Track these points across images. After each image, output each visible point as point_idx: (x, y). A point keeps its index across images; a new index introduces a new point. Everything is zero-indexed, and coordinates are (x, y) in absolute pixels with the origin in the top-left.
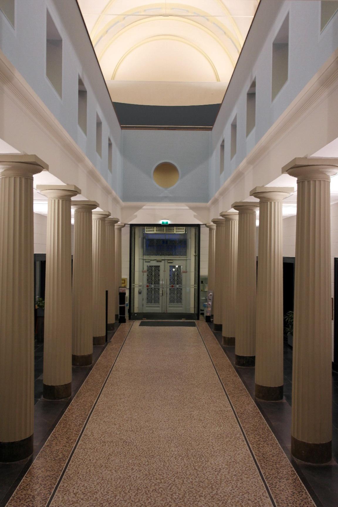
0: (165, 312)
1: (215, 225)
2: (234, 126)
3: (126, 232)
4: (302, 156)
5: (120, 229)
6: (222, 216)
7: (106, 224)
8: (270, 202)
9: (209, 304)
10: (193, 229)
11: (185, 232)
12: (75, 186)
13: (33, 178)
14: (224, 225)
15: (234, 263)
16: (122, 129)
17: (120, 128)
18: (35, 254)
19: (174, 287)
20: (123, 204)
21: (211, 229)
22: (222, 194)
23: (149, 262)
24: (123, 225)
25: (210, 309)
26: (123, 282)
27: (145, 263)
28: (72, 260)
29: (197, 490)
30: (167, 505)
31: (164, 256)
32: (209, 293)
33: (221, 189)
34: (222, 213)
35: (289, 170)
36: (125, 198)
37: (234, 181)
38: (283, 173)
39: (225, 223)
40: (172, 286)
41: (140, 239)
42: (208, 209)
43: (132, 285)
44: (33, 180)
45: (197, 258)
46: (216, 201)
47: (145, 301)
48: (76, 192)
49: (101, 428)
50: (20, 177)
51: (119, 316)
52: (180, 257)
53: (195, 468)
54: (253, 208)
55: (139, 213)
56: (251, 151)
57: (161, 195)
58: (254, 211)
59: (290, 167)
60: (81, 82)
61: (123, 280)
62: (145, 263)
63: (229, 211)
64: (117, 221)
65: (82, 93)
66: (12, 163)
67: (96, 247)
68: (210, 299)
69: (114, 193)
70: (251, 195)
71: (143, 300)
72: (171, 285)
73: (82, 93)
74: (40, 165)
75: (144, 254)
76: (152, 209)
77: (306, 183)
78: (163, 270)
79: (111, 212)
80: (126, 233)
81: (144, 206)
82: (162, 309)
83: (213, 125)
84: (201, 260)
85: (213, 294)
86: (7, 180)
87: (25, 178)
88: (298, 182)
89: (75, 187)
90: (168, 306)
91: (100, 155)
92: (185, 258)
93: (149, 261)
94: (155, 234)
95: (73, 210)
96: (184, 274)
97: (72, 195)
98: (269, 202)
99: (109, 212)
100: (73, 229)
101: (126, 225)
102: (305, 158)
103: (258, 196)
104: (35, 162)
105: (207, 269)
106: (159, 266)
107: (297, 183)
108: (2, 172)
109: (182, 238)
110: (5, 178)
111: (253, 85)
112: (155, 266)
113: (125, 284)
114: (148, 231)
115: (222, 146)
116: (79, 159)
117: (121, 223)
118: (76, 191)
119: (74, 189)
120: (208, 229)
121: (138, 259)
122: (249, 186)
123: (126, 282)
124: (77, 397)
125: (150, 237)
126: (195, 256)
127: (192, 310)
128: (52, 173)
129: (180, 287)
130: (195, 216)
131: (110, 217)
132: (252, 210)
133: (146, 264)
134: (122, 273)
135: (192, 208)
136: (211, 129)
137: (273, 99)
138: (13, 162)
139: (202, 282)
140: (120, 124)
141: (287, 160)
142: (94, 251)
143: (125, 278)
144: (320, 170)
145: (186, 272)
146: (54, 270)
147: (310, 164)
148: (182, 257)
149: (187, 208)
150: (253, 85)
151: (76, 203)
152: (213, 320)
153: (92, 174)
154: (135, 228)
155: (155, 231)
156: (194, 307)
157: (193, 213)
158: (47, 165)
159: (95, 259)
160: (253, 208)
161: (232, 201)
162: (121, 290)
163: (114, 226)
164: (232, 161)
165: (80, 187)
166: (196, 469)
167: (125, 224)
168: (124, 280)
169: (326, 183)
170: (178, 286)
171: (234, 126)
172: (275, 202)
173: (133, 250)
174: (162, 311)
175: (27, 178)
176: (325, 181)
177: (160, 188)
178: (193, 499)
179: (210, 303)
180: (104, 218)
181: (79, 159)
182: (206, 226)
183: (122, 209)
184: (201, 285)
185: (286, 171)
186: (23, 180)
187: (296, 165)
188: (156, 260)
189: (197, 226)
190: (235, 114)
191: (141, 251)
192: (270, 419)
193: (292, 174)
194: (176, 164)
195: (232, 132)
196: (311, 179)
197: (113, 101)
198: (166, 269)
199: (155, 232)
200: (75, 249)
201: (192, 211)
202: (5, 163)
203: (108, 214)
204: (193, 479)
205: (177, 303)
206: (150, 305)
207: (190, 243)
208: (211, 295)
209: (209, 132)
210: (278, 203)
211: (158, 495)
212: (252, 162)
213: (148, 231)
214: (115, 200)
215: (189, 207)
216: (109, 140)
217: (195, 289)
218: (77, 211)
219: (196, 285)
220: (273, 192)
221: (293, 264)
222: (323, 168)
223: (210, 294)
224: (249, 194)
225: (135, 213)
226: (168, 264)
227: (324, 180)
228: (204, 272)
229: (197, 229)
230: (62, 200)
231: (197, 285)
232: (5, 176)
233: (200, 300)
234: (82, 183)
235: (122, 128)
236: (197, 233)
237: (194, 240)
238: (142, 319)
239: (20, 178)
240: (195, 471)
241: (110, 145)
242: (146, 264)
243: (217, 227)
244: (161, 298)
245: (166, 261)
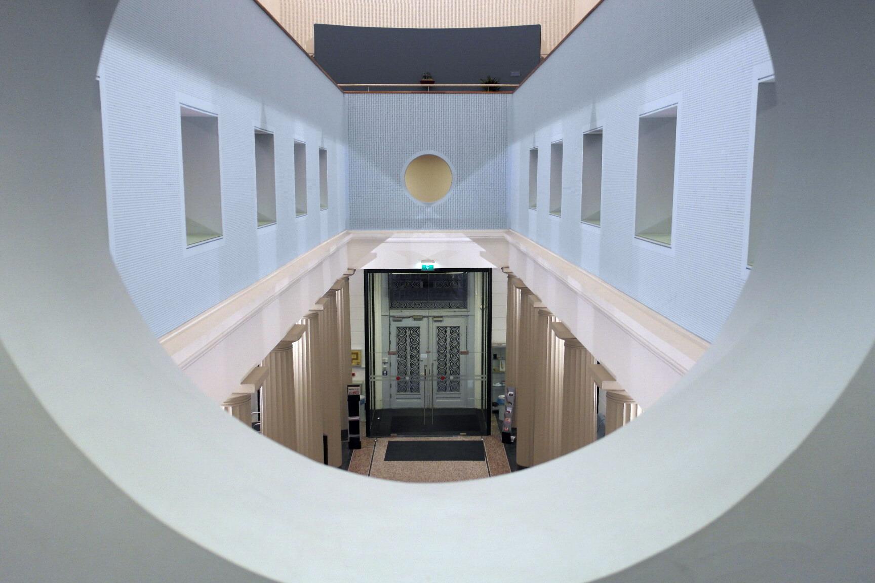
0: (431, 407)
8: (627, 404)
9: (509, 412)
15: (554, 383)
19: (445, 380)
23: (401, 321)
25: (510, 420)
26: (355, 356)
27: (392, 323)
32: (508, 392)
40: (443, 378)
43: (370, 376)
45: (486, 312)
47: (394, 389)
52: (455, 312)
55: (379, 250)
57: (420, 217)
61: (353, 353)
62: (392, 323)
68: (510, 403)
71: (391, 387)
72: (440, 376)
75: (391, 307)
76: (405, 242)
78: (426, 350)
81: (389, 237)
82: (425, 402)
84: (493, 328)
85: (515, 392)
90: (435, 396)
92: (465, 314)
93: (400, 319)
105: (505, 332)
106: (419, 328)
112: (410, 328)
113: (359, 361)
121: (381, 317)
123: (359, 358)
126: (483, 310)
127: (477, 402)
129: (455, 380)
130: (482, 254)
133: (395, 325)
135: (477, 240)
139: (495, 356)
142: (299, 420)
143: (357, 350)
145: (466, 353)
149: (468, 239)
152: (515, 440)
156: (481, 398)
162: (353, 390)
168: (357, 354)
170: (452, 378)
173: (371, 298)
174: (425, 406)
177: (419, 203)
179: (510, 409)
184: (494, 363)
188: (412, 317)
198: (430, 346)
201: (476, 244)
205: (451, 391)
206: (403, 395)
208: (512, 395)
217: (482, 382)
219: (485, 376)
223: (510, 393)
225: (374, 248)
228: (499, 336)
231: (486, 376)
233: (492, 387)
237: (481, 280)
238: (390, 435)
242: (395, 325)
244: (422, 383)
245: (431, 319)
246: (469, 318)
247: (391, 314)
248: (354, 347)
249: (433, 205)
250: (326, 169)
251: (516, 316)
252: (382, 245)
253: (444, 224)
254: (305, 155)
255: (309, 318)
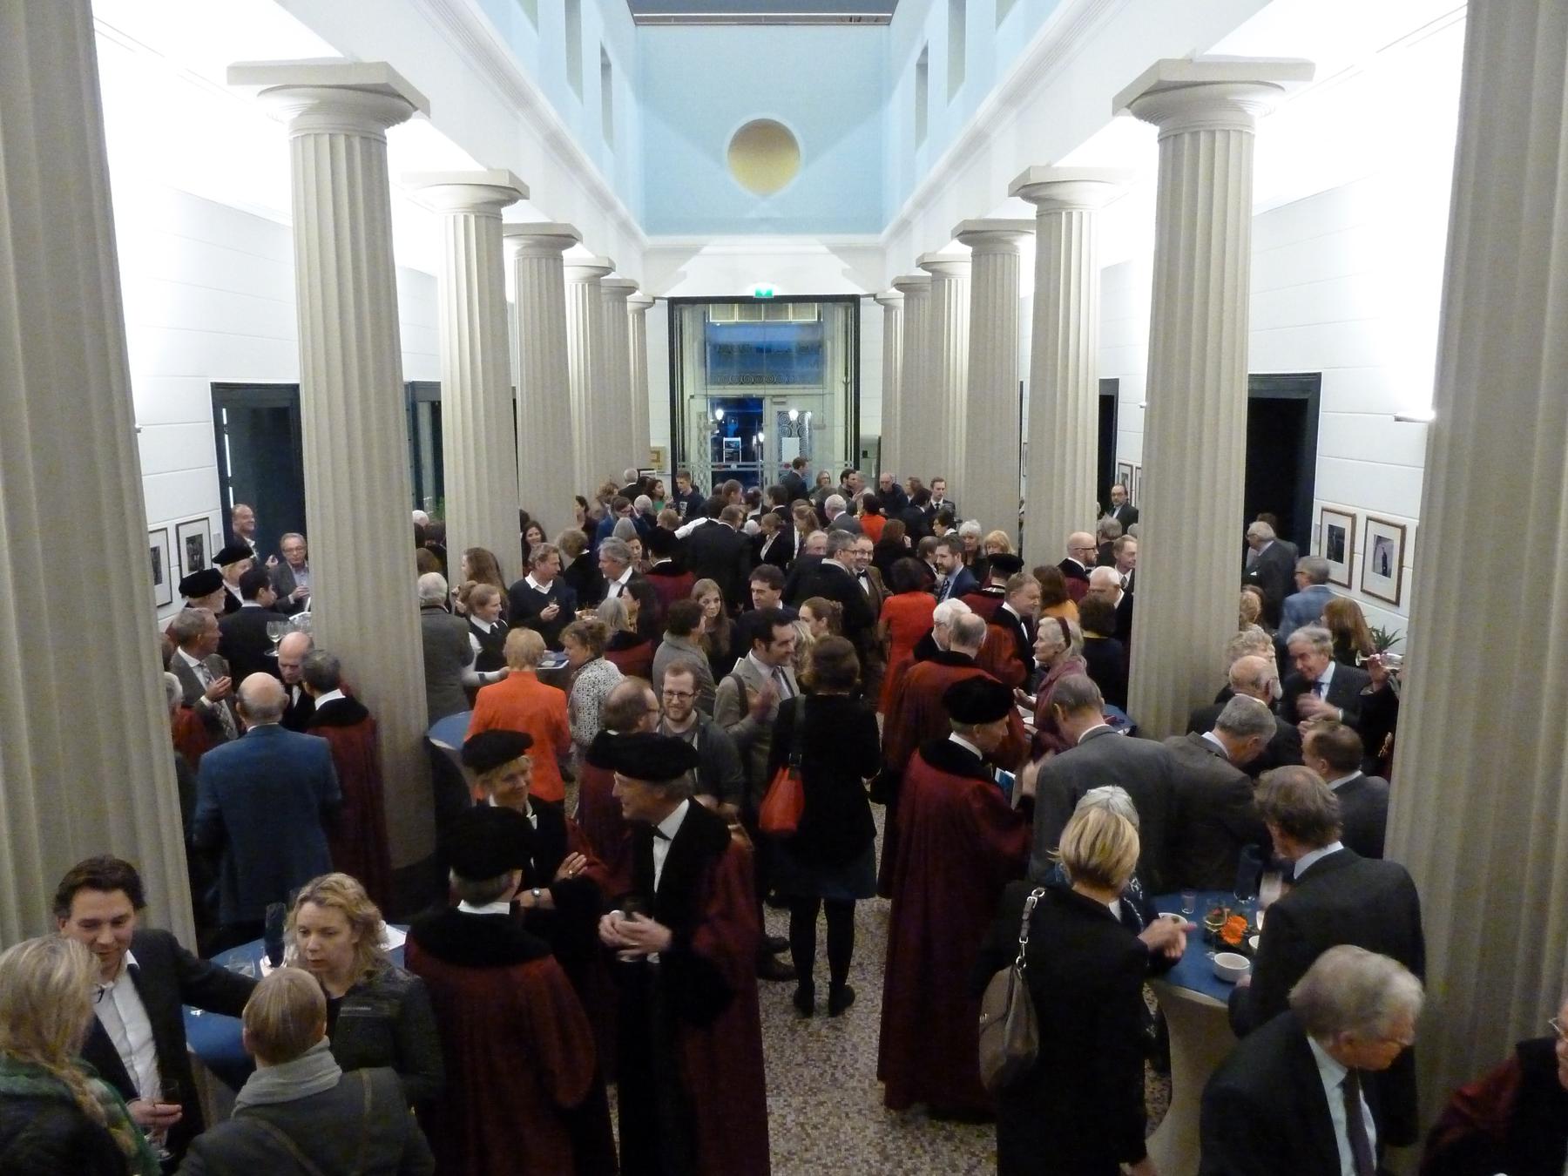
3: (658, 319)
4: (1179, 54)
5: (641, 313)
6: (924, 265)
7: (603, 296)
8: (1067, 214)
10: (840, 310)
11: (819, 318)
12: (511, 174)
14: (928, 294)
20: (649, 241)
21: (888, 308)
24: (651, 300)
28: (514, 401)
29: (876, 985)
30: (799, 1022)
33: (919, 190)
34: (923, 256)
35: (1138, 101)
36: (653, 227)
37: (958, 161)
38: (1115, 112)
39: (930, 288)
41: (696, 344)
42: (881, 251)
46: (905, 226)
48: (512, 193)
50: (348, 133)
51: (741, 463)
53: (867, 929)
54: (1011, 238)
55: (691, 266)
56: (1008, 74)
58: (1016, 246)
59: (1143, 91)
61: (653, 452)
64: (631, 289)
66: (319, 90)
70: (1012, 195)
77: (1187, 138)
81: (705, 245)
83: (892, 10)
86: (311, 142)
87: (362, 138)
88: (1163, 140)
91: (580, 92)
92: (821, 391)
94: (737, 325)
96: (816, 433)
97: (505, 200)
98: (1064, 213)
100: (513, 317)
101: (656, 301)
104: (386, 85)
107: (1160, 141)
110: (302, 136)
114: (717, 317)
115: (922, 67)
116: (519, 98)
120: (883, 307)
122: (1006, 166)
124: (787, 1160)
126: (846, 384)
130: (844, 273)
132: (1009, 242)
135: (837, 250)
136: (888, 21)
139: (865, 454)
141: (1130, 70)
143: (660, 448)
145: (822, 427)
146: (465, 440)
147: (1207, 79)
149: (824, 249)
151: (519, 231)
153: (556, 144)
154: (681, 309)
155: (735, 316)
158: (425, 98)
159: (576, 393)
160: (1011, 238)
163: (625, 302)
165: (525, 178)
166: (871, 932)
167: (654, 299)
168: (657, 452)
176: (1241, 132)
178: (866, 1007)
180: (597, 277)
181: (519, 98)
183: (647, 254)
185: (1128, 107)
189: (851, 302)
191: (700, 372)
193: (1146, 114)
194: (788, 124)
199: (736, 319)
200: (522, 375)
203: (606, 264)
204: (863, 956)
211: (775, 1000)
212: (1014, 97)
213: (717, 317)
214: (624, 226)
215: (828, 247)
218: (523, 256)
220: (1073, 183)
222: (1013, 235)
224: (1006, 191)
226: (773, 406)
227: (1238, 128)
228: (871, 428)
230: (476, 217)
232: (302, 136)
234: (531, 167)
235: (638, 21)
236: (851, 323)
239: (346, 135)
240: (869, 936)
241: (606, 67)
243: (907, 299)
246: (828, 397)
247: (710, 392)
248: (654, 444)
251: (896, 368)
254: (580, 42)
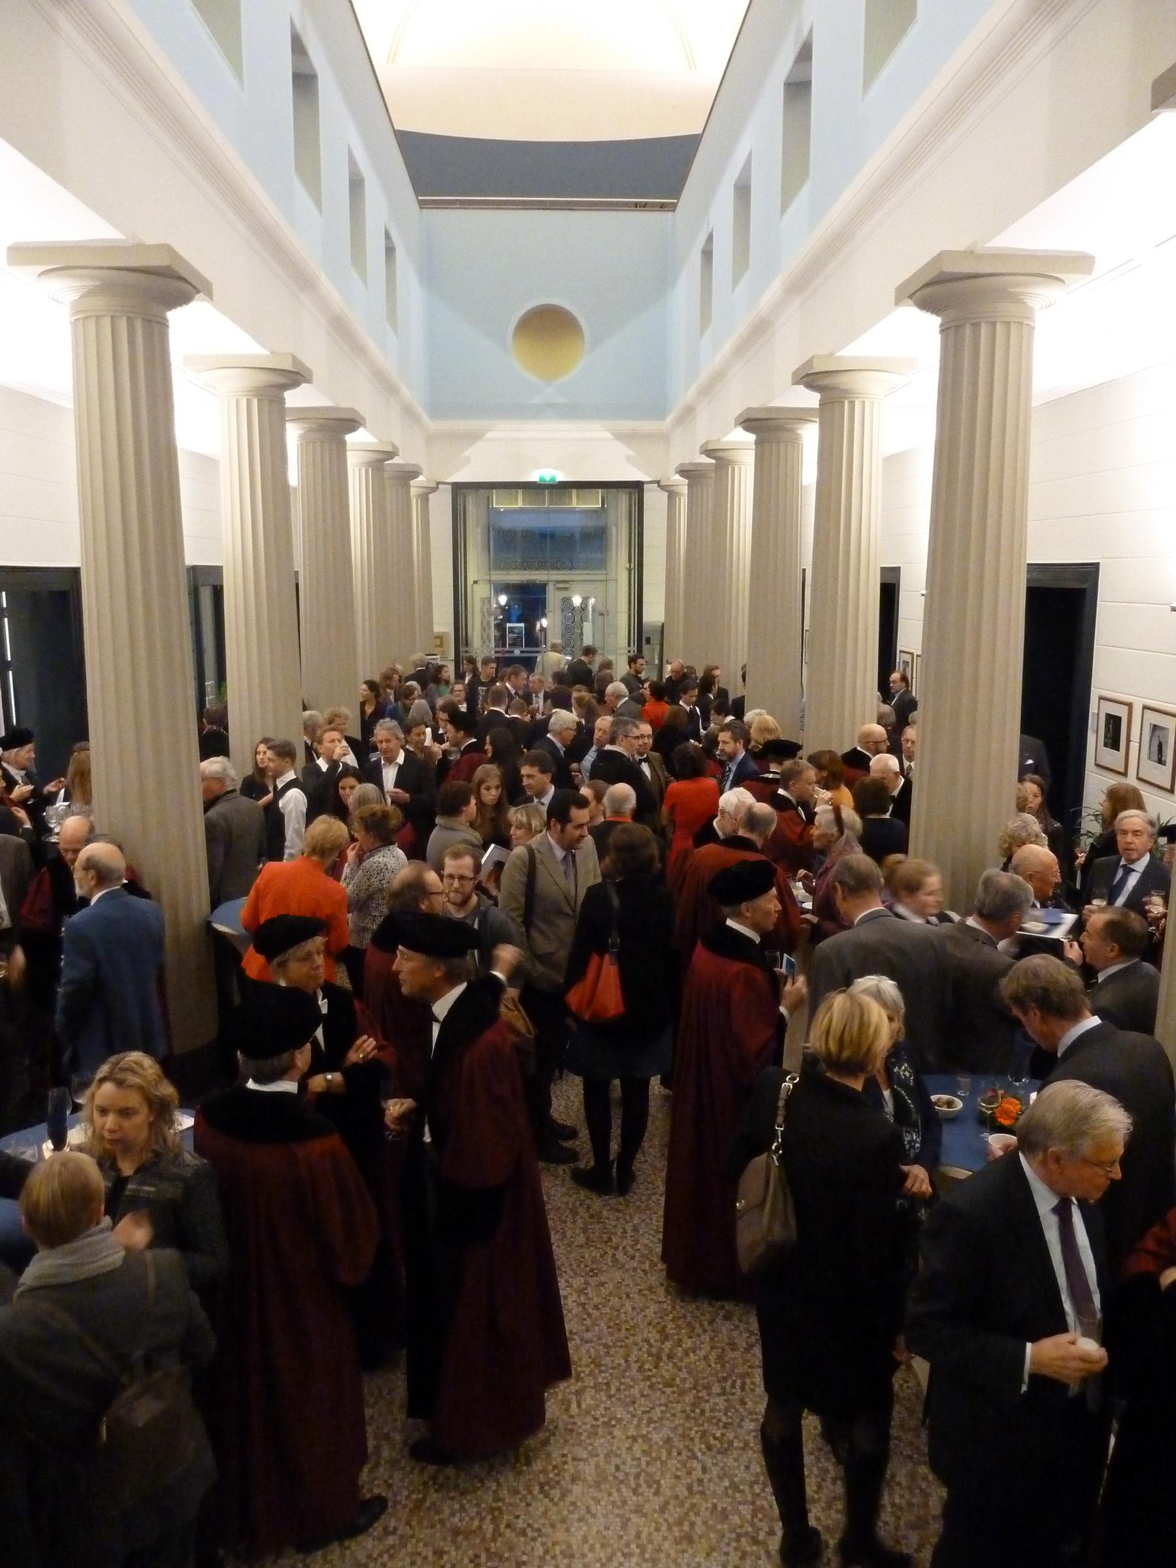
1: (686, 481)
2: (743, 191)
3: (441, 504)
5: (424, 498)
12: (295, 359)
13: (166, 320)
14: (711, 482)
16: (421, 208)
17: (416, 207)
18: (194, 569)
20: (432, 425)
21: (672, 495)
22: (708, 390)
24: (434, 485)
28: (297, 585)
31: (546, 572)
36: (438, 410)
38: (898, 302)
42: (664, 438)
43: (461, 649)
44: (167, 326)
48: (295, 377)
49: (652, 1425)
50: (131, 315)
57: (536, 400)
60: (298, 47)
63: (725, 439)
64: (415, 474)
65: (304, 81)
67: (361, 546)
69: (406, 392)
70: (796, 383)
73: (304, 81)
74: (185, 280)
79: (398, 444)
80: (441, 507)
83: (678, 196)
86: (92, 324)
89: (295, 360)
91: (363, 275)
92: (603, 577)
95: (293, 434)
98: (846, 402)
99: (394, 446)
102: (970, 253)
103: (815, 384)
104: (169, 267)
107: (942, 331)
108: (75, 301)
109: (591, 523)
111: (805, 54)
114: (500, 503)
115: (707, 254)
116: (303, 281)
117: (428, 480)
118: (297, 373)
119: (293, 366)
123: (445, 645)
125: (506, 524)
126: (630, 570)
128: (224, 310)
130: (628, 459)
131: (396, 460)
132: (792, 430)
134: (435, 620)
135: (620, 436)
136: (672, 208)
137: (868, 81)
138: (102, 268)
140: (418, 191)
144: (1011, 290)
148: (594, 572)
149: (608, 435)
150: (805, 54)
151: (302, 415)
153: (340, 327)
157: (622, 450)
161: (737, 408)
163: (408, 487)
164: (786, 217)
167: (438, 483)
168: (440, 638)
169: (1025, 330)
171: (743, 191)
172: (864, 402)
175: (150, 321)
180: (379, 462)
181: (303, 281)
182: (659, 486)
183: (431, 439)
185: (910, 297)
186: (138, 325)
187: (942, 273)
190: (746, 153)
192: (1016, 1012)
195: (736, 214)
196: (984, 318)
197: (397, 127)
199: (520, 505)
202: (78, 272)
203: (389, 449)
207: (614, 538)
209: (667, 216)
210: (873, 403)
212: (800, 284)
213: (500, 503)
214: (408, 412)
215: (613, 434)
216: (388, 236)
221: (894, 585)
222: (1017, 285)
228: (654, 613)
229: (635, 497)
235: (423, 204)
236: (635, 509)
241: (390, 250)
243: (690, 486)
247: (493, 578)
249: (658, 1139)
250: (363, 212)
252: (479, 444)
253: (571, 411)
255: (255, 396)
